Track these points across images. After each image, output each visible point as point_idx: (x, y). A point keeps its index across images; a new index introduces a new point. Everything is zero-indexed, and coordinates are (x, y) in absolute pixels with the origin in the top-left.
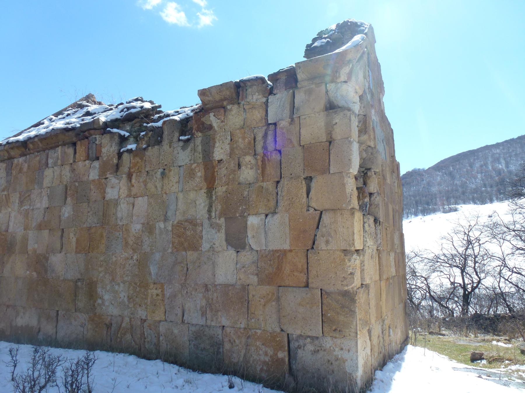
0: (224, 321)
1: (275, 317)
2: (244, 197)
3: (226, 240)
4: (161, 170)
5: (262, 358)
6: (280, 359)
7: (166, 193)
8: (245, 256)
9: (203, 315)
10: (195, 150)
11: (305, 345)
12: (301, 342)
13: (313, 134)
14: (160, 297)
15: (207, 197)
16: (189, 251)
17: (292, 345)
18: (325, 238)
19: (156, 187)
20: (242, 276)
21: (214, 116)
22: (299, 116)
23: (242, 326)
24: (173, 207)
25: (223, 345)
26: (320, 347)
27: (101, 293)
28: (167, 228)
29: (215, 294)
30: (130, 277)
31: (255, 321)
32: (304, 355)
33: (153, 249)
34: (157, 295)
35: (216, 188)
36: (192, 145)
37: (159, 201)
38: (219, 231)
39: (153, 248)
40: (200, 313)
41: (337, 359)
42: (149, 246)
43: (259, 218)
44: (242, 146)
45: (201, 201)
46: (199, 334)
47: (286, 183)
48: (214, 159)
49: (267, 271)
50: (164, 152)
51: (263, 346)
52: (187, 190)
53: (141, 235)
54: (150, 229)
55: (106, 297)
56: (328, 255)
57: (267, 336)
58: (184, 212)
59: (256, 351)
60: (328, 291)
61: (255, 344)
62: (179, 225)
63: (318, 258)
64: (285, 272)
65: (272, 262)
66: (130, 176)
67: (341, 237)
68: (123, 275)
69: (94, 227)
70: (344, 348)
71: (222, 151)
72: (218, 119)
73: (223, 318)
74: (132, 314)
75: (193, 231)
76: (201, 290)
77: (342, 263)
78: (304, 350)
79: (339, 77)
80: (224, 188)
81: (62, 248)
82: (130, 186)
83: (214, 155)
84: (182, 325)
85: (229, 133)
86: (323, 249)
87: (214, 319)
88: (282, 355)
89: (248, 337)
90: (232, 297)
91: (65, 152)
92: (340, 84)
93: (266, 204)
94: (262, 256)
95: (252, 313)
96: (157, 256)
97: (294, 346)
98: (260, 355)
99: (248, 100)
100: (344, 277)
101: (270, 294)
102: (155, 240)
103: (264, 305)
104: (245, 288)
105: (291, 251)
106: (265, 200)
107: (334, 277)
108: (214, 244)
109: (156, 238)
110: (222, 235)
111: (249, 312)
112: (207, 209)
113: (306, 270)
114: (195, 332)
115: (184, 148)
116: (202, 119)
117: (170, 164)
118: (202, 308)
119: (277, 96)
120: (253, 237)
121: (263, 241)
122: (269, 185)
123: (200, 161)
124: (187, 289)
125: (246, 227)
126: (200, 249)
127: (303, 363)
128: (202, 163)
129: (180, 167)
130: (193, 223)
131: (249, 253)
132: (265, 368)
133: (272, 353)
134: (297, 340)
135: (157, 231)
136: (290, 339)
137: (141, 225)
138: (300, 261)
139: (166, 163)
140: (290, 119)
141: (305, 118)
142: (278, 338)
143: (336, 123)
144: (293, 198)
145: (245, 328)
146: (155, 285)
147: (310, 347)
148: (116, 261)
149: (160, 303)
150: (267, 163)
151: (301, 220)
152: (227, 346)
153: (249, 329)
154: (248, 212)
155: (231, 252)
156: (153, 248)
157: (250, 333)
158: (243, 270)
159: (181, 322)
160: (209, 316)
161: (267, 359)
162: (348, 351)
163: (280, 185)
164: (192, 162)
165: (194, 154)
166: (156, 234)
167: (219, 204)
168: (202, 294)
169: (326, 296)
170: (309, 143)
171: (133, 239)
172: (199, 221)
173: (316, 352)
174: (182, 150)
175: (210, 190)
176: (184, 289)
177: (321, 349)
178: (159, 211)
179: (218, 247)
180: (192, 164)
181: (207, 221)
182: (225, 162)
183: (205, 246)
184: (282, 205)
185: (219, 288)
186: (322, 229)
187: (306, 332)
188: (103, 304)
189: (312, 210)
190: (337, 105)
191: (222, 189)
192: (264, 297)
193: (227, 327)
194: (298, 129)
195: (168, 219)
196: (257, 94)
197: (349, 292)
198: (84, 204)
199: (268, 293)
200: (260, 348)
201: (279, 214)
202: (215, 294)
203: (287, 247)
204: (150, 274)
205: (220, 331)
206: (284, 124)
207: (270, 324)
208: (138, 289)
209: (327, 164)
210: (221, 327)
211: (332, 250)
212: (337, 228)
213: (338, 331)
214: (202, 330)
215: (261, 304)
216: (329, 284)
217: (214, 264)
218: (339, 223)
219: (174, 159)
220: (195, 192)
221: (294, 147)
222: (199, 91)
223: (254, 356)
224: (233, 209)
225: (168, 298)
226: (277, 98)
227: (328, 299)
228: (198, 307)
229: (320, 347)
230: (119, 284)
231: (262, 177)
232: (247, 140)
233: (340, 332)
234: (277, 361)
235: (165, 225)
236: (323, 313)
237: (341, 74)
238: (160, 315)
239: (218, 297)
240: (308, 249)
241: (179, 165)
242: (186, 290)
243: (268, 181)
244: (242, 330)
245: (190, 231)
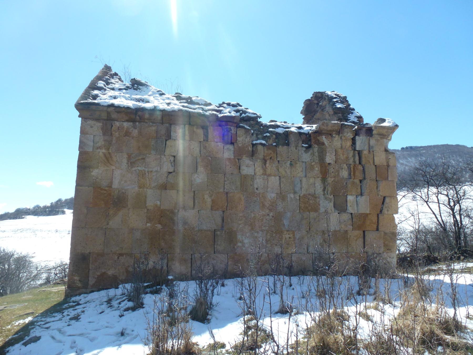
4: (289, 162)
10: (314, 155)
14: (292, 239)
16: (312, 212)
21: (325, 138)
24: (299, 185)
27: (241, 239)
30: (267, 227)
34: (290, 238)
38: (331, 202)
42: (282, 208)
44: (342, 158)
45: (318, 184)
49: (357, 224)
52: (309, 176)
53: (275, 201)
54: (283, 197)
55: (246, 241)
58: (307, 190)
66: (265, 161)
68: (261, 226)
69: (232, 192)
74: (270, 251)
80: (332, 179)
81: (194, 207)
82: (265, 169)
83: (326, 160)
91: (194, 131)
96: (289, 214)
103: (356, 240)
104: (346, 232)
105: (370, 214)
110: (332, 204)
115: (306, 152)
116: (318, 138)
121: (356, 208)
123: (317, 161)
125: (346, 201)
126: (319, 211)
130: (314, 196)
135: (289, 199)
137: (276, 195)
138: (375, 219)
146: (288, 232)
148: (254, 216)
158: (344, 223)
165: (313, 157)
171: (269, 203)
172: (318, 195)
175: (324, 180)
176: (309, 234)
181: (323, 196)
183: (322, 210)
186: (386, 205)
188: (243, 246)
189: (380, 196)
194: (372, 156)
198: (220, 174)
203: (368, 212)
204: (284, 225)
206: (366, 152)
208: (274, 235)
209: (387, 176)
220: (314, 179)
221: (371, 165)
230: (258, 232)
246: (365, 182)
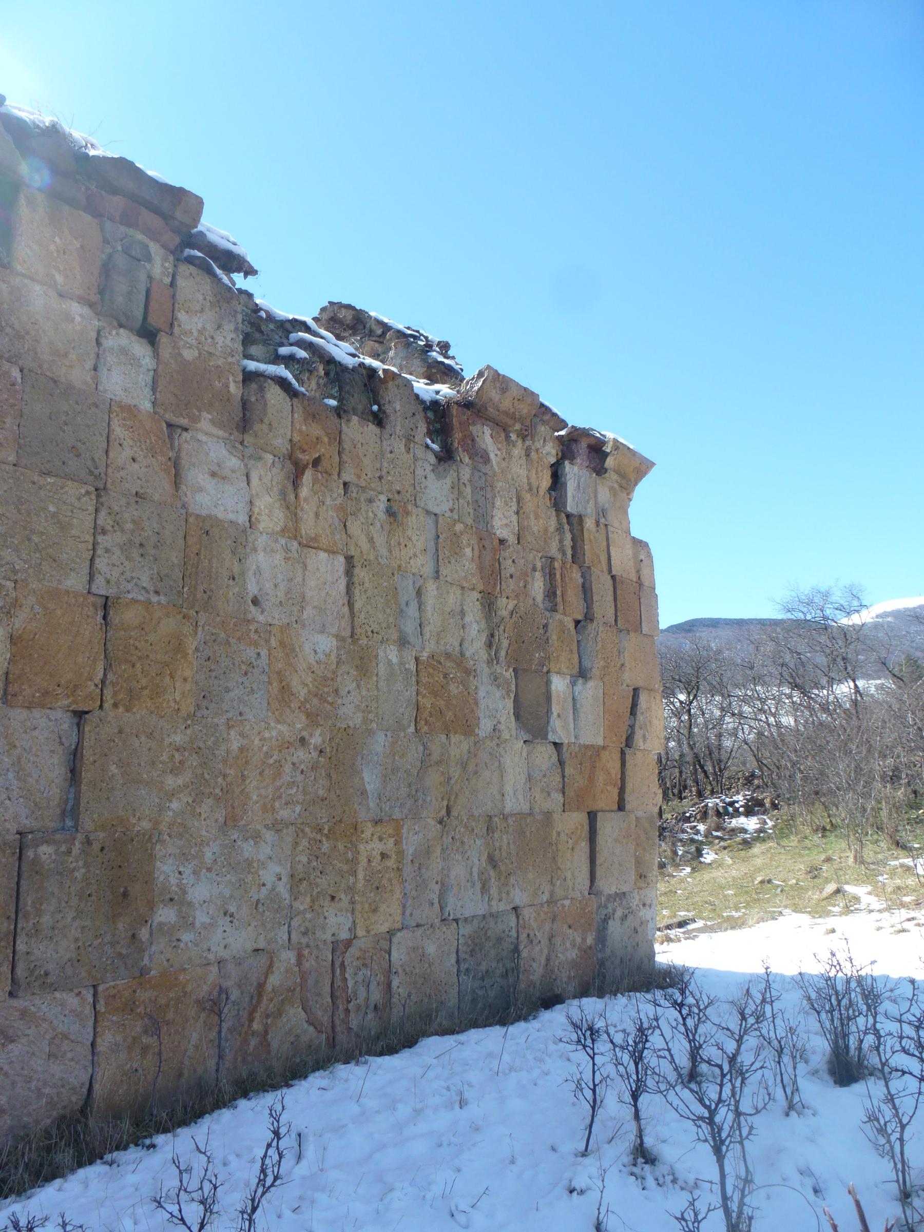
0: (519, 897)
3: (517, 716)
14: (391, 863)
19: (371, 540)
33: (372, 721)
37: (385, 584)
39: (371, 716)
51: (571, 931)
105: (604, 748)
121: (572, 726)
135: (382, 669)
149: (390, 880)
183: (485, 727)
203: (600, 741)
235: (401, 657)
246: (591, 628)
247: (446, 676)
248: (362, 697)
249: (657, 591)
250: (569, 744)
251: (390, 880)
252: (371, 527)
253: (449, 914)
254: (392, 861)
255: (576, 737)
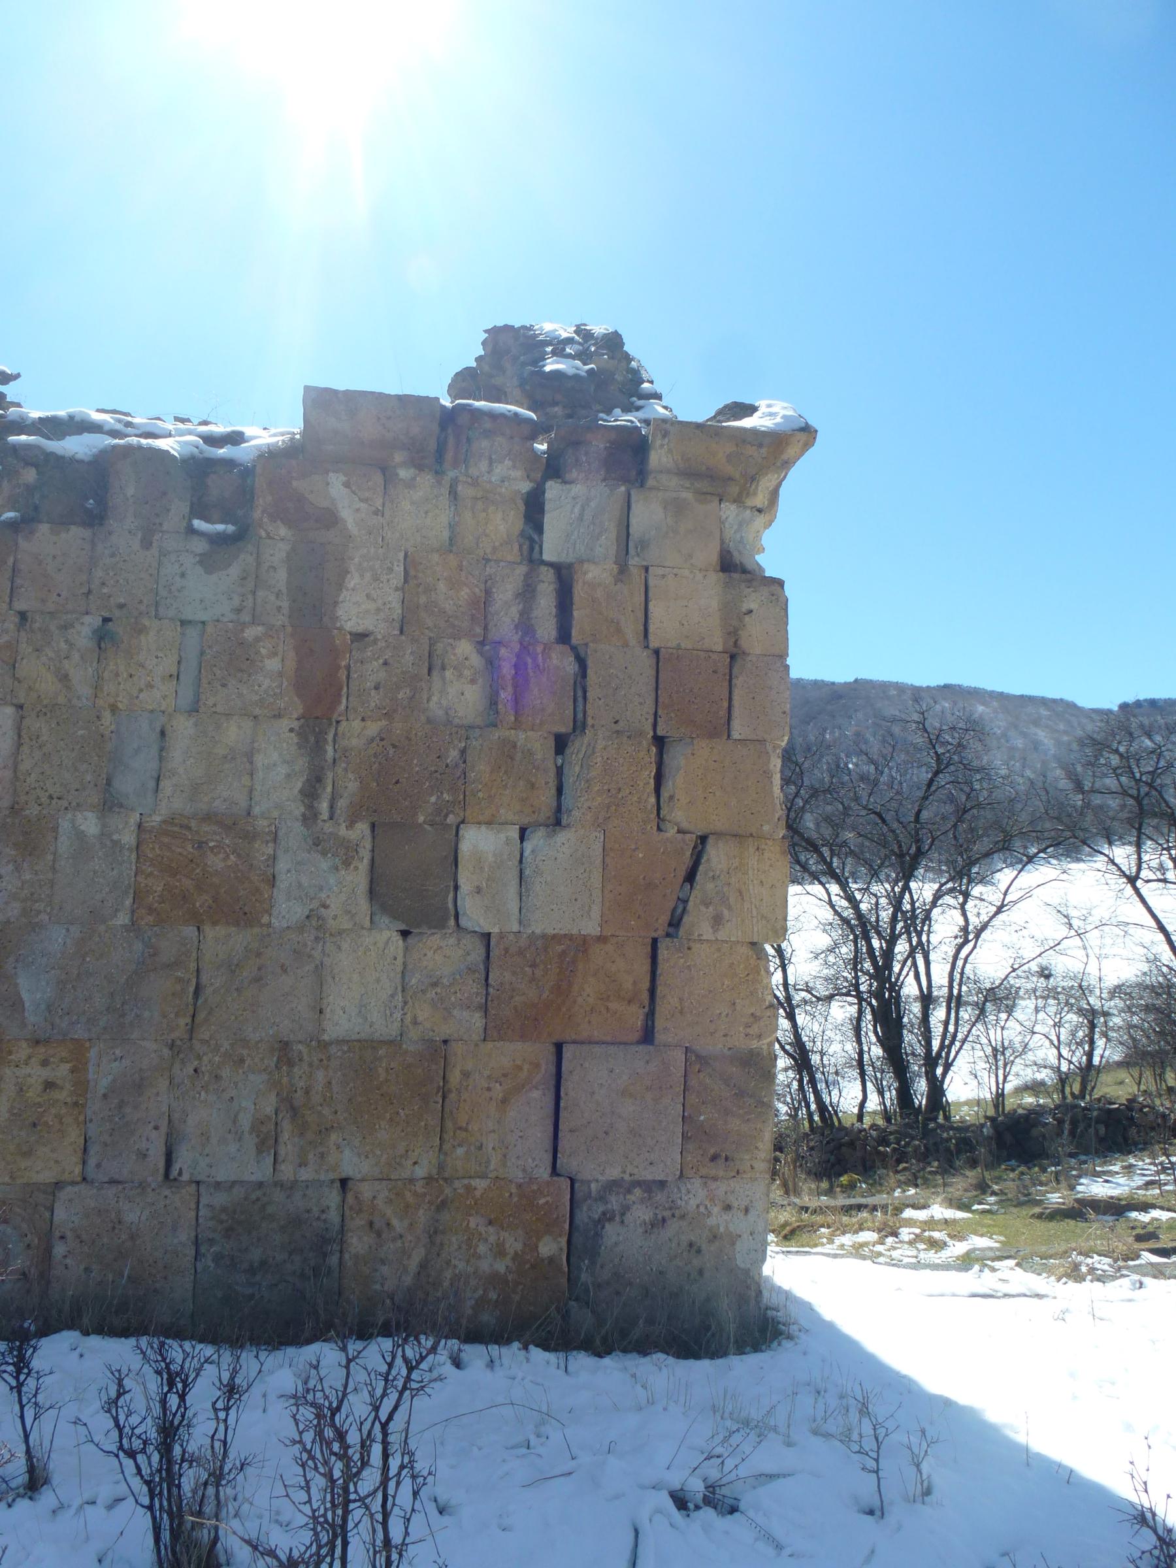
0: (350, 1163)
1: (539, 1135)
2: (447, 766)
3: (372, 893)
5: (485, 1266)
6: (543, 1260)
7: (114, 709)
8: (438, 949)
9: (260, 1148)
11: (625, 1209)
12: (614, 1202)
13: (686, 623)
14: (62, 1095)
15: (300, 746)
17: (582, 1216)
18: (711, 908)
19: (64, 678)
20: (424, 1013)
21: (347, 485)
22: (645, 563)
23: (420, 1172)
25: (342, 1242)
26: (671, 1209)
28: (115, 837)
29: (320, 1075)
31: (467, 1152)
32: (621, 1238)
33: (39, 912)
34: (49, 1085)
35: (338, 722)
36: (246, 559)
37: (81, 732)
39: (39, 906)
40: (250, 1142)
41: (715, 1237)
43: (502, 836)
46: (243, 1217)
47: (601, 744)
48: (338, 625)
50: (113, 555)
51: (491, 1229)
56: (715, 956)
57: (507, 1195)
59: (464, 1246)
60: (704, 1055)
61: (465, 1224)
62: (176, 829)
63: (685, 962)
64: (580, 1000)
65: (539, 972)
67: (754, 910)
70: (735, 1204)
71: (371, 606)
72: (361, 500)
73: (347, 1152)
75: (239, 856)
76: (262, 1059)
77: (751, 977)
78: (622, 1222)
79: (755, 494)
80: (373, 728)
83: (340, 612)
84: (167, 1192)
85: (401, 555)
86: (704, 937)
87: (311, 1156)
88: (550, 1247)
89: (442, 1206)
90: (387, 1081)
92: (748, 512)
93: (524, 795)
94: (506, 950)
95: (460, 1128)
97: (590, 1217)
98: (480, 1257)
99: (473, 471)
100: (752, 1014)
101: (526, 1067)
102: (50, 875)
103: (504, 1101)
105: (602, 939)
106: (521, 783)
107: (727, 1015)
108: (325, 907)
109: (54, 869)
110: (358, 878)
111: (449, 1124)
112: (299, 785)
113: (645, 996)
114: (224, 1209)
115: (208, 563)
117: (143, 608)
118: (257, 1124)
119: (577, 489)
120: (478, 893)
121: (513, 906)
122: (538, 744)
123: (280, 620)
124: (199, 1058)
126: (265, 919)
127: (617, 1261)
128: (289, 629)
129: (183, 623)
131: (452, 941)
132: (493, 1295)
133: (519, 1246)
134: (602, 1198)
135: (64, 844)
136: (579, 1195)
139: (122, 601)
140: (615, 566)
141: (663, 576)
142: (545, 1196)
143: (751, 611)
144: (620, 790)
145: (429, 1179)
147: (641, 1214)
149: (59, 1118)
150: (531, 674)
151: (640, 855)
152: (358, 1243)
153: (445, 1180)
154: (462, 815)
155: (386, 934)
156: (39, 906)
157: (448, 1191)
158: (431, 994)
159: (160, 1178)
160: (289, 1145)
161: (501, 1267)
162: (743, 1212)
163: (578, 748)
164: (246, 617)
165: (254, 593)
166: (55, 854)
167: (351, 776)
168: (265, 1077)
169: (697, 1067)
170: (674, 644)
172: (265, 823)
173: (658, 1223)
174: (199, 570)
177: (673, 1216)
178: (76, 769)
179: (336, 916)
180: (244, 626)
181: (298, 827)
182: (381, 644)
184: (585, 806)
185: (339, 1054)
187: (636, 1171)
189: (672, 832)
190: (741, 563)
191: (364, 728)
192: (505, 1075)
193: (363, 1180)
195: (121, 806)
196: (508, 463)
197: (758, 1054)
199: (519, 1063)
200: (481, 1234)
201: (573, 829)
202: (320, 1075)
203: (591, 927)
205: (332, 1198)
207: (518, 1157)
209: (723, 713)
210: (338, 1184)
211: (726, 942)
212: (745, 883)
213: (723, 1160)
214: (258, 1199)
215: (491, 1099)
216: (712, 1034)
217: (319, 969)
218: (750, 872)
219: (163, 593)
222: (307, 389)
223: (457, 1263)
224: (405, 799)
225: (105, 1096)
226: (572, 494)
227: (702, 1075)
228: (245, 1122)
229: (671, 1209)
231: (512, 712)
232: (468, 591)
233: (728, 1163)
234: (533, 1267)
235: (104, 826)
236: (686, 1114)
237: (760, 488)
238: (57, 1162)
239: (330, 1083)
240: (656, 936)
241: (183, 617)
242: (196, 1063)
243: (533, 730)
244: (419, 1187)
245: (222, 856)
247: (200, 845)
248: (23, 883)
249: (789, 661)
250: (502, 935)
251: (59, 1118)
252: (66, 662)
253: (180, 1174)
254: (65, 1093)
255: (520, 923)
